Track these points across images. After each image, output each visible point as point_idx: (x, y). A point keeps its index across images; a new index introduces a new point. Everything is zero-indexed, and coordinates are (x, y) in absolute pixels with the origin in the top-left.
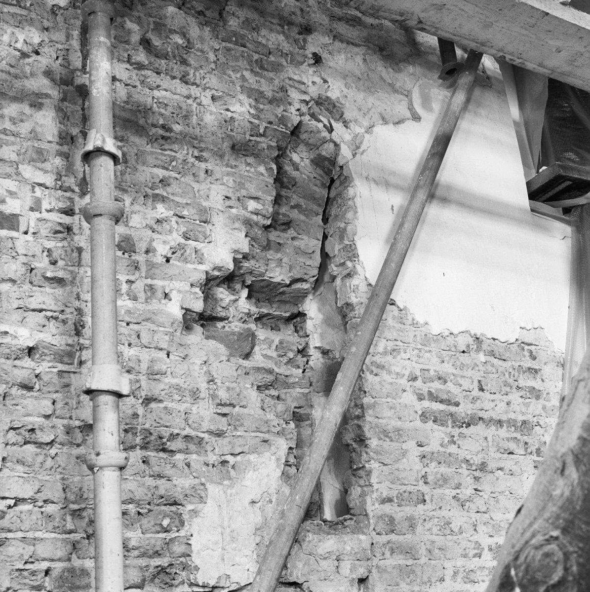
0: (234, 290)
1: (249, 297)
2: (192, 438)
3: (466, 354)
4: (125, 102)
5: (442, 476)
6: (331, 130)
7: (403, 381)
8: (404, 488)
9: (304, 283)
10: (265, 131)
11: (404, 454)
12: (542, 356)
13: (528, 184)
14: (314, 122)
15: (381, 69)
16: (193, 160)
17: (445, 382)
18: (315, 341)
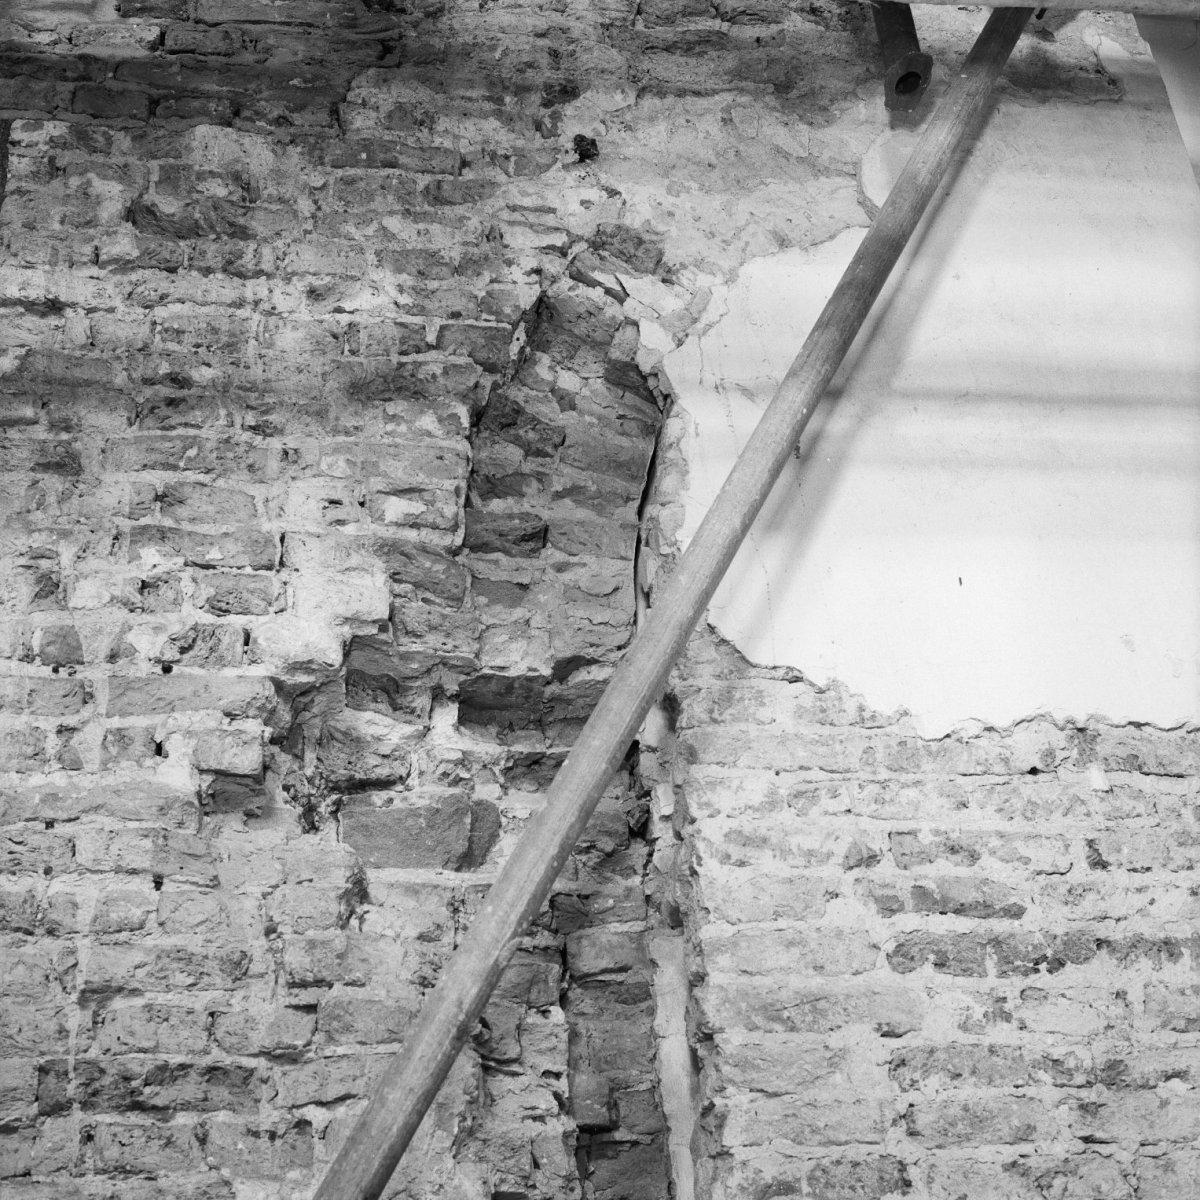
0: (413, 712)
1: (463, 720)
2: (225, 1072)
3: (1040, 777)
4: (83, 347)
5: (966, 1109)
7: (831, 872)
8: (836, 1152)
9: (594, 668)
10: (440, 337)
14: (583, 290)
15: (774, 130)
16: (246, 436)
17: (974, 857)
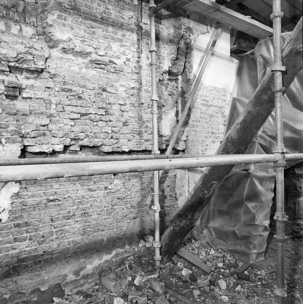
6: (190, 36)
11: (198, 112)
12: (227, 92)
13: (231, 49)
18: (180, 85)
